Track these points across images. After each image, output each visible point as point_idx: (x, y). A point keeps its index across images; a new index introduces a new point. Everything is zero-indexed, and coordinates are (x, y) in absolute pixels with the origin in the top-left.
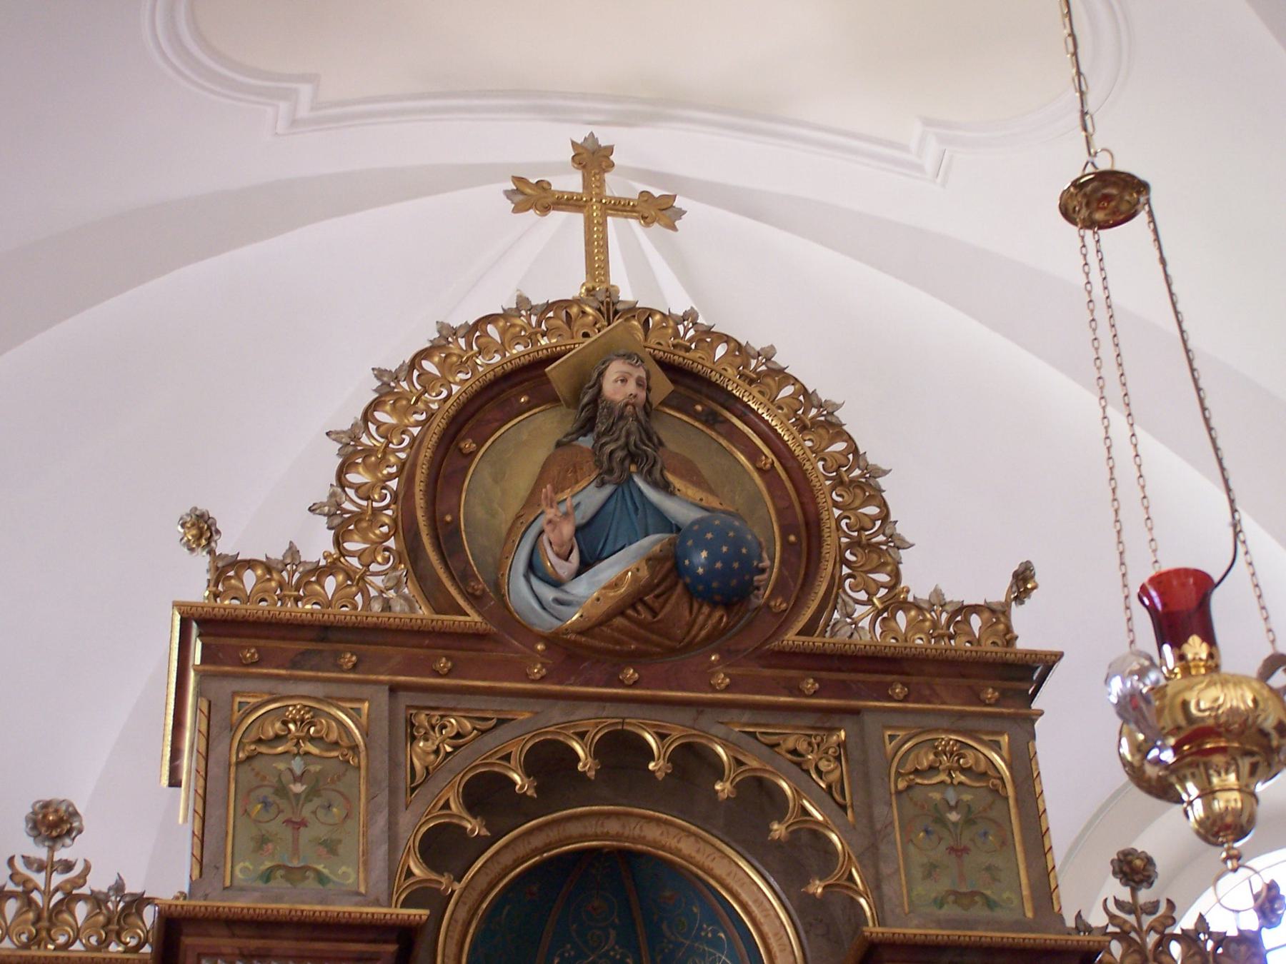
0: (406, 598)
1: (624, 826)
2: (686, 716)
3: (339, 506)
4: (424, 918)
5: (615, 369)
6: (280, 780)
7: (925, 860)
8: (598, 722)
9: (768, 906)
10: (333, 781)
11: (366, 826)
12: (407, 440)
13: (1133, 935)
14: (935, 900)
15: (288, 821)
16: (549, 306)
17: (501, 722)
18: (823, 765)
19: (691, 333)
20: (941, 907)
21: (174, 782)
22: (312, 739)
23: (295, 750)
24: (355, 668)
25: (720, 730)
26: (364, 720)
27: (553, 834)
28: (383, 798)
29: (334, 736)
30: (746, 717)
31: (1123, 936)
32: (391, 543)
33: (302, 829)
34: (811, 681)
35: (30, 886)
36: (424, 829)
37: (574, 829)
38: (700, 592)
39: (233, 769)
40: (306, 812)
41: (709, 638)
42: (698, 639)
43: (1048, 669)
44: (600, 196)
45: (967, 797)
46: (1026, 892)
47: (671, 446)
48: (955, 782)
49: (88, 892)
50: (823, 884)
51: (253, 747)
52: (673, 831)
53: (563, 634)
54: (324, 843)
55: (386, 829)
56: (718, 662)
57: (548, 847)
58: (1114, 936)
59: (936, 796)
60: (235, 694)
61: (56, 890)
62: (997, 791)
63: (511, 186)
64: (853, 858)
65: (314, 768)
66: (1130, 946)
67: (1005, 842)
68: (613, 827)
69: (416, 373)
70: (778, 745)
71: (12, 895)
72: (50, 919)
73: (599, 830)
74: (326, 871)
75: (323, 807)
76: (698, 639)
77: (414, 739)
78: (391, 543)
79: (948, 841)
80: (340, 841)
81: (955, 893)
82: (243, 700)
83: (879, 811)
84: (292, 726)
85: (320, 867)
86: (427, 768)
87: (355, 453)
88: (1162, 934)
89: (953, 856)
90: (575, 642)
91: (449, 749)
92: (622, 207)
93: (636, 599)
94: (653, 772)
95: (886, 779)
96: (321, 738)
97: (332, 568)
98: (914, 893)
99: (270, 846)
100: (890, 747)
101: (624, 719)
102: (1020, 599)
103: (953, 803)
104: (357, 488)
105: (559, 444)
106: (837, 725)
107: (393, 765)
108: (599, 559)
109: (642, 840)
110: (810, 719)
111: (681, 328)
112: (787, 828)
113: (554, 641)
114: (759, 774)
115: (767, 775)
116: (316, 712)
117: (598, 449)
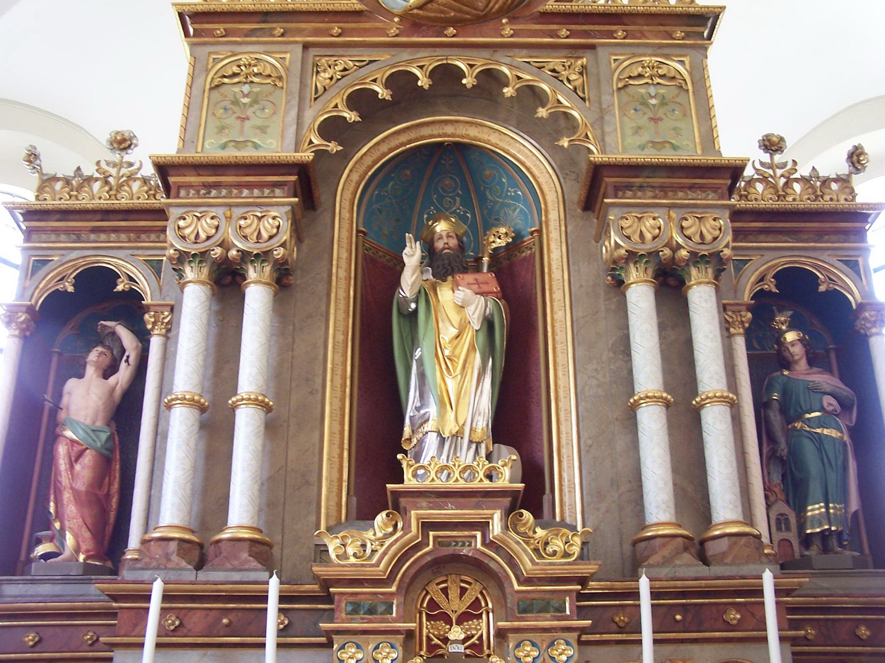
1: (456, 129)
2: (486, 53)
4: (311, 158)
6: (235, 97)
7: (634, 125)
9: (542, 167)
10: (267, 96)
11: (284, 117)
13: (770, 179)
14: (639, 147)
15: (238, 118)
18: (573, 77)
20: (643, 149)
22: (256, 75)
23: (245, 80)
24: (282, 35)
25: (508, 60)
26: (287, 63)
27: (412, 135)
29: (267, 72)
31: (764, 179)
33: (247, 122)
34: (565, 30)
35: (107, 174)
36: (322, 119)
37: (426, 131)
39: (206, 94)
40: (249, 112)
42: (494, 10)
43: (717, 17)
45: (662, 91)
46: (697, 140)
48: (655, 83)
49: (140, 176)
50: (568, 139)
51: (219, 79)
52: (486, 130)
53: (411, 10)
54: (259, 128)
55: (296, 118)
56: (507, 23)
57: (410, 142)
58: (758, 180)
59: (642, 91)
60: (210, 53)
61: (122, 176)
62: (682, 87)
64: (588, 125)
65: (256, 89)
66: (767, 185)
67: (686, 114)
70: (544, 67)
71: (97, 180)
72: (117, 191)
73: (441, 132)
74: (259, 142)
75: (259, 109)
76: (494, 10)
77: (318, 72)
79: (650, 114)
80: (268, 126)
81: (652, 142)
82: (215, 57)
83: (605, 98)
84: (243, 68)
85: (255, 141)
86: (325, 88)
88: (788, 178)
89: (652, 122)
90: (417, 14)
91: (339, 77)
94: (465, 85)
95: (611, 81)
96: (261, 74)
98: (626, 143)
99: (227, 131)
100: (613, 65)
101: (447, 56)
103: (653, 94)
106: (581, 55)
109: (467, 136)
110: (565, 52)
112: (547, 110)
114: (531, 83)
115: (536, 84)
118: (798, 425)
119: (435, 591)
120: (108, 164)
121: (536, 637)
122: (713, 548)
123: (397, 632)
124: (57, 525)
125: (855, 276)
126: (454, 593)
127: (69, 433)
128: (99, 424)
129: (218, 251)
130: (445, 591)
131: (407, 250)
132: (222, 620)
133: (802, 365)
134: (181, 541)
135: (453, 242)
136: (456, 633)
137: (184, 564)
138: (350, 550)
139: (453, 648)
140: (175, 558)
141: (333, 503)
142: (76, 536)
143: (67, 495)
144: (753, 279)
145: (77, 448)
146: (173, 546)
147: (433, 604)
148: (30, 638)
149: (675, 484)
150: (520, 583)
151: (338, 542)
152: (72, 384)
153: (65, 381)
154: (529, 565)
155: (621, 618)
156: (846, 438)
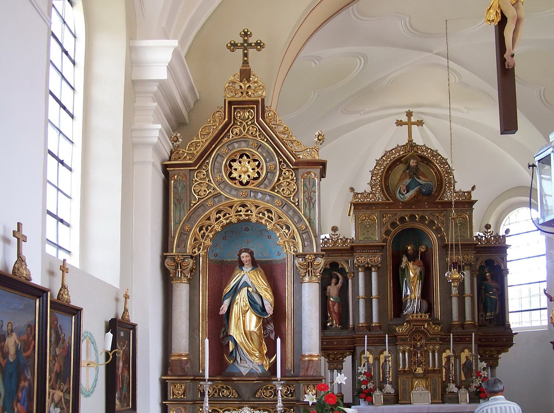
0: (382, 197)
3: (371, 183)
5: (412, 161)
8: (409, 214)
12: (381, 171)
16: (402, 146)
17: (395, 215)
19: (424, 148)
21: (349, 215)
24: (375, 209)
28: (379, 227)
30: (430, 212)
32: (379, 188)
38: (423, 194)
44: (411, 122)
45: (462, 222)
47: (420, 169)
63: (396, 121)
65: (370, 223)
68: (412, 225)
69: (382, 160)
77: (383, 218)
78: (379, 188)
87: (374, 174)
93: (415, 197)
97: (371, 193)
102: (473, 190)
104: (374, 180)
105: (404, 171)
107: (381, 222)
111: (423, 148)
113: (402, 202)
116: (370, 215)
117: (409, 173)
118: (487, 295)
119: (414, 336)
120: (332, 234)
121: (432, 344)
122: (465, 326)
123: (409, 344)
125: (503, 262)
126: (417, 336)
127: (332, 299)
128: (337, 297)
130: (416, 335)
131: (403, 258)
132: (327, 324)
133: (490, 280)
135: (412, 251)
136: (418, 343)
137: (367, 331)
138: (400, 330)
140: (365, 330)
141: (391, 315)
142: (335, 321)
143: (333, 313)
146: (365, 327)
148: (335, 343)
149: (459, 311)
151: (398, 328)
152: (329, 287)
154: (432, 332)
155: (447, 340)
156: (497, 298)
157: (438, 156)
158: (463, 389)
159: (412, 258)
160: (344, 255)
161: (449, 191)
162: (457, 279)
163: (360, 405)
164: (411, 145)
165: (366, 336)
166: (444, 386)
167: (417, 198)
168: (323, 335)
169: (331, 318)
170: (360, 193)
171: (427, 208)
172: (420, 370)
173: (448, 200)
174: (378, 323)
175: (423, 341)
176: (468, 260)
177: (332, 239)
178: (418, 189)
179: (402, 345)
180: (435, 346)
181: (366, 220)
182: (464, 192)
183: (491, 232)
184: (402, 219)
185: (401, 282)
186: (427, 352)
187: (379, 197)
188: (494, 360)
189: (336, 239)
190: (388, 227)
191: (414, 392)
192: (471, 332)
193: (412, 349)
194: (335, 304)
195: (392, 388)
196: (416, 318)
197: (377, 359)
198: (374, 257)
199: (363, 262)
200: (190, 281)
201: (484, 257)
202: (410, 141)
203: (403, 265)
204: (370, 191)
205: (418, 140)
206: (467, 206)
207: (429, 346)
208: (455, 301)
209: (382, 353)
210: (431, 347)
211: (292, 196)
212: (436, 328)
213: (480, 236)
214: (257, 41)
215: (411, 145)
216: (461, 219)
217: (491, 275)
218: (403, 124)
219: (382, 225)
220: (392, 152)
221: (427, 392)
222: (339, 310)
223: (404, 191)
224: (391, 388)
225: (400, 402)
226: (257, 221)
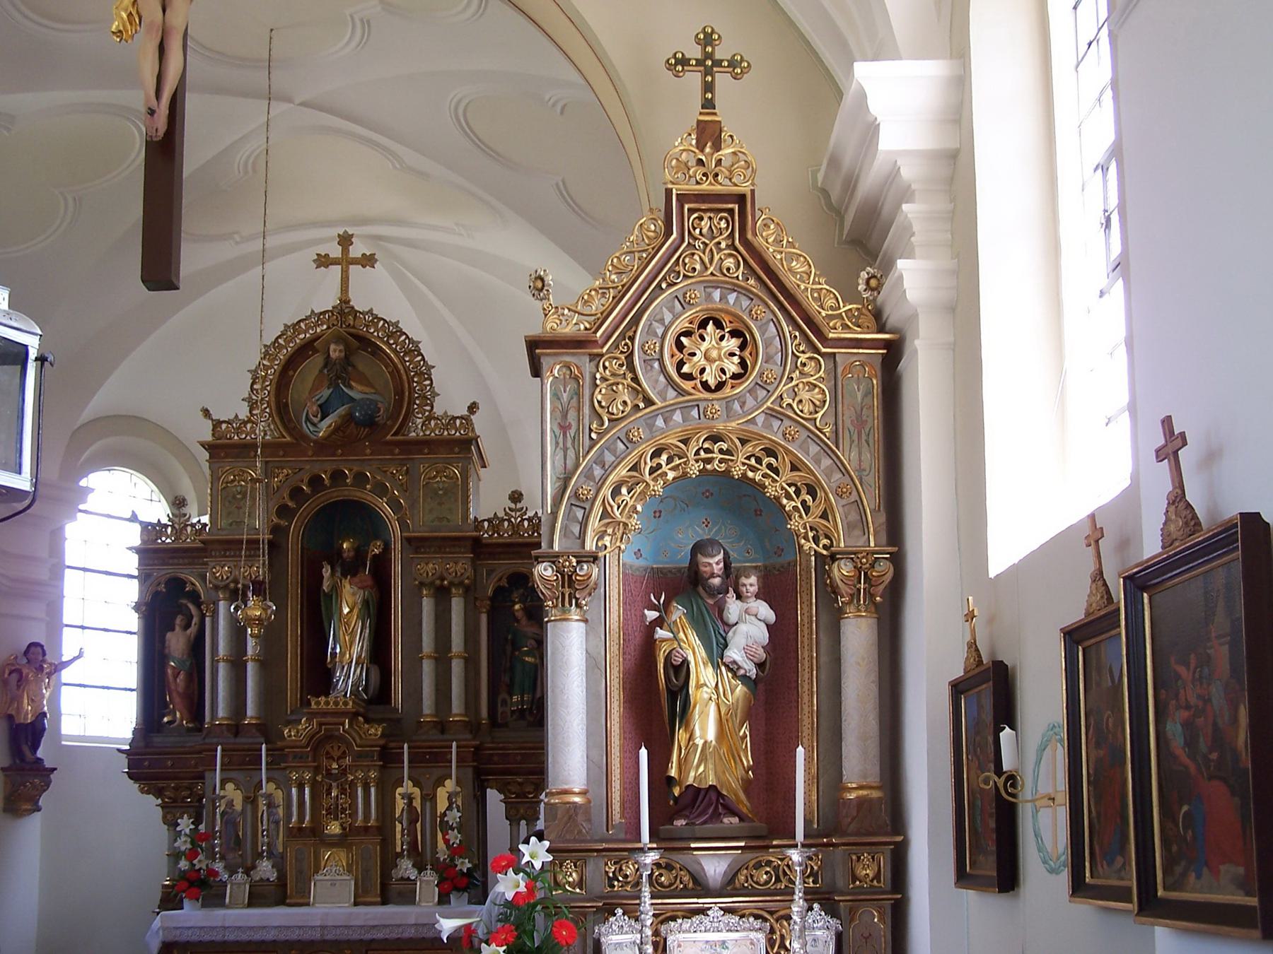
0: (271, 430)
3: (251, 397)
5: (332, 347)
8: (330, 467)
12: (273, 370)
17: (300, 470)
37: (335, 494)
38: (360, 424)
40: (242, 503)
41: (365, 437)
59: (436, 485)
63: (316, 257)
67: (456, 500)
92: (355, 261)
97: (249, 421)
102: (473, 413)
108: (327, 416)
111: (367, 317)
113: (315, 442)
116: (244, 472)
119: (328, 747)
123: (375, 765)
124: (171, 706)
126: (336, 748)
127: (173, 664)
129: (232, 585)
130: (332, 747)
131: (324, 570)
133: (524, 621)
134: (227, 724)
138: (293, 734)
139: (334, 772)
140: (225, 732)
143: (174, 694)
144: (495, 580)
145: (177, 671)
146: (224, 727)
147: (328, 753)
148: (169, 763)
150: (357, 746)
152: (169, 635)
153: (165, 636)
157: (400, 336)
158: (429, 872)
159: (350, 569)
160: (196, 561)
161: (420, 416)
162: (257, 620)
163: (182, 908)
164: (344, 309)
165: (219, 748)
166: (389, 861)
167: (344, 433)
168: (142, 744)
169: (171, 706)
170: (458, 417)
171: (398, 455)
172: (334, 828)
173: (418, 435)
174: (257, 718)
175: (348, 761)
176: (456, 574)
177: (509, 521)
178: (343, 413)
179: (296, 769)
180: (369, 771)
181: (236, 483)
182: (455, 418)
183: (523, 508)
184: (315, 481)
185: (326, 624)
186: (353, 784)
187: (264, 431)
188: (528, 805)
189: (519, 519)
190: (284, 498)
191: (320, 878)
192: (211, 744)
193: (319, 778)
194: (179, 673)
195: (273, 867)
196: (324, 707)
197: (251, 800)
198: (250, 567)
199: (225, 577)
200: (212, 616)
201: (506, 566)
202: (345, 301)
203: (326, 586)
204: (247, 417)
205: (359, 303)
206: (457, 450)
207: (356, 771)
208: (427, 667)
209: (440, 782)
210: (360, 775)
211: (819, 415)
212: (372, 731)
213: (498, 518)
214: (734, 55)
215: (344, 309)
216: (444, 479)
217: (524, 609)
218: (331, 264)
219: (270, 492)
220: (300, 327)
221: (348, 878)
222: (187, 687)
223: (316, 417)
224: (270, 867)
225: (288, 901)
226: (744, 475)
